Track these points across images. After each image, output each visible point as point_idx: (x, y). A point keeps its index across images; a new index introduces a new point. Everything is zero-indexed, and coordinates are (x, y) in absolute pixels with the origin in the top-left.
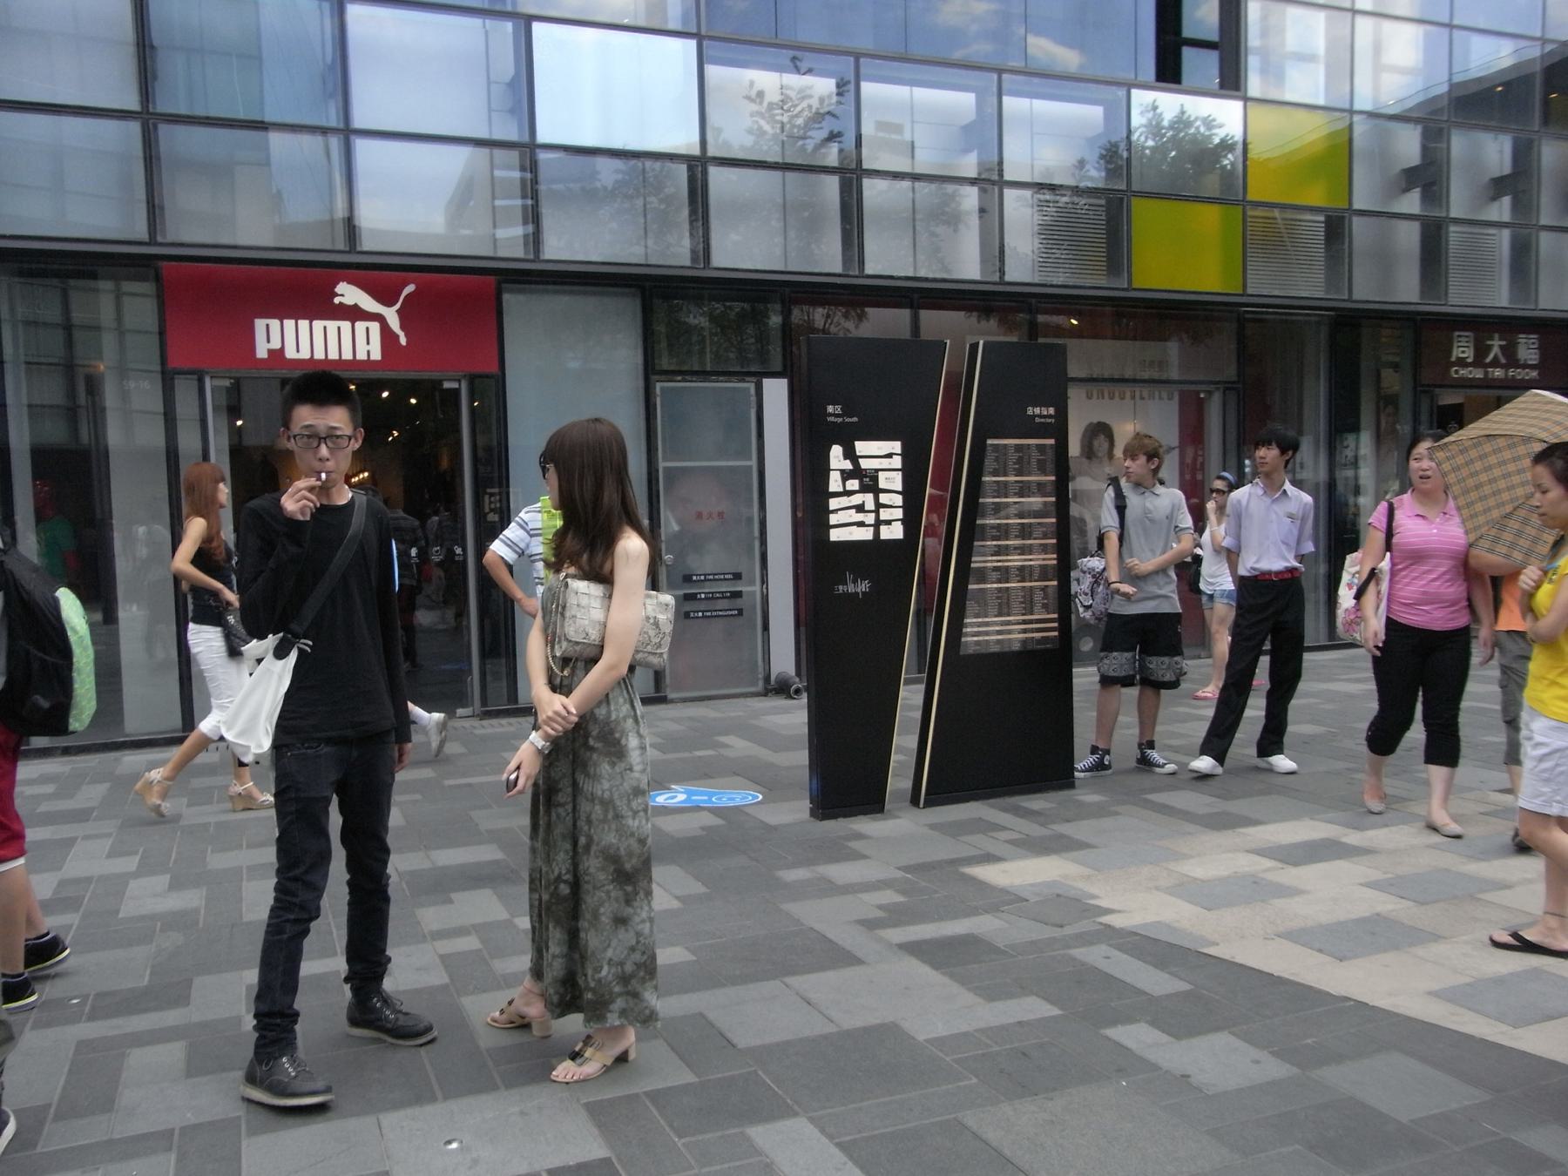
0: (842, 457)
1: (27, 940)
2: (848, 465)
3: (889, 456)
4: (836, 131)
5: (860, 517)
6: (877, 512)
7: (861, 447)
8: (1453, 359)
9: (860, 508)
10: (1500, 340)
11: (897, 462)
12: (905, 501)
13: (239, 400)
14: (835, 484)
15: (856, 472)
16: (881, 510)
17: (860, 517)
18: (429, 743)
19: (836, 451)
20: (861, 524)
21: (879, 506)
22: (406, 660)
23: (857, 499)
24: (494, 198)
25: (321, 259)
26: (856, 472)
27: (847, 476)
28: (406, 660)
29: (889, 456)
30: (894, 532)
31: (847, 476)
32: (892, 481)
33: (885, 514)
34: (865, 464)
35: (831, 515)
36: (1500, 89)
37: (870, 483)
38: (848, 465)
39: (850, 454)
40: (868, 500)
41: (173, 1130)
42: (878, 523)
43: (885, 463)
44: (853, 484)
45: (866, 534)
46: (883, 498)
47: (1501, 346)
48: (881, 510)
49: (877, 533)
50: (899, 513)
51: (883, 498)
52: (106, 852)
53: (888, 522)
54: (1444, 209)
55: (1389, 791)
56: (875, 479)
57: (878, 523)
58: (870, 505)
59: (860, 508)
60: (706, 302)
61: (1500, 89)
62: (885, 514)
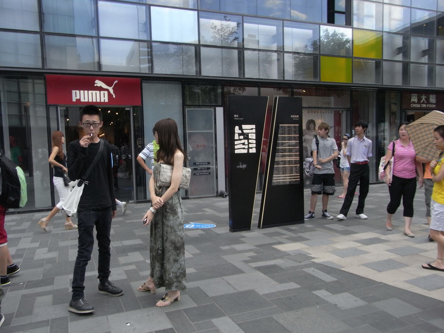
0: (238, 130)
1: (8, 266)
2: (240, 132)
3: (252, 129)
4: (237, 37)
5: (243, 146)
6: (248, 145)
7: (244, 127)
8: (412, 102)
9: (244, 144)
10: (425, 96)
11: (254, 131)
12: (256, 142)
13: (68, 113)
14: (236, 137)
15: (242, 134)
16: (250, 144)
17: (243, 146)
19: (237, 128)
20: (244, 148)
21: (249, 143)
22: (115, 187)
23: (243, 141)
25: (91, 73)
26: (242, 134)
27: (240, 135)
28: (115, 187)
29: (252, 129)
30: (253, 151)
31: (240, 135)
32: (253, 136)
33: (250, 146)
34: (245, 131)
35: (235, 146)
36: (425, 25)
37: (246, 137)
38: (240, 132)
39: (241, 129)
40: (246, 142)
41: (49, 320)
42: (249, 148)
43: (251, 131)
44: (242, 137)
45: (245, 151)
46: (250, 141)
47: (425, 98)
48: (250, 144)
49: (248, 151)
50: (255, 145)
51: (250, 141)
52: (30, 241)
53: (252, 148)
54: (409, 59)
56: (248, 136)
57: (249, 148)
58: (246, 143)
59: (244, 144)
60: (200, 86)
61: (425, 25)
62: (250, 146)
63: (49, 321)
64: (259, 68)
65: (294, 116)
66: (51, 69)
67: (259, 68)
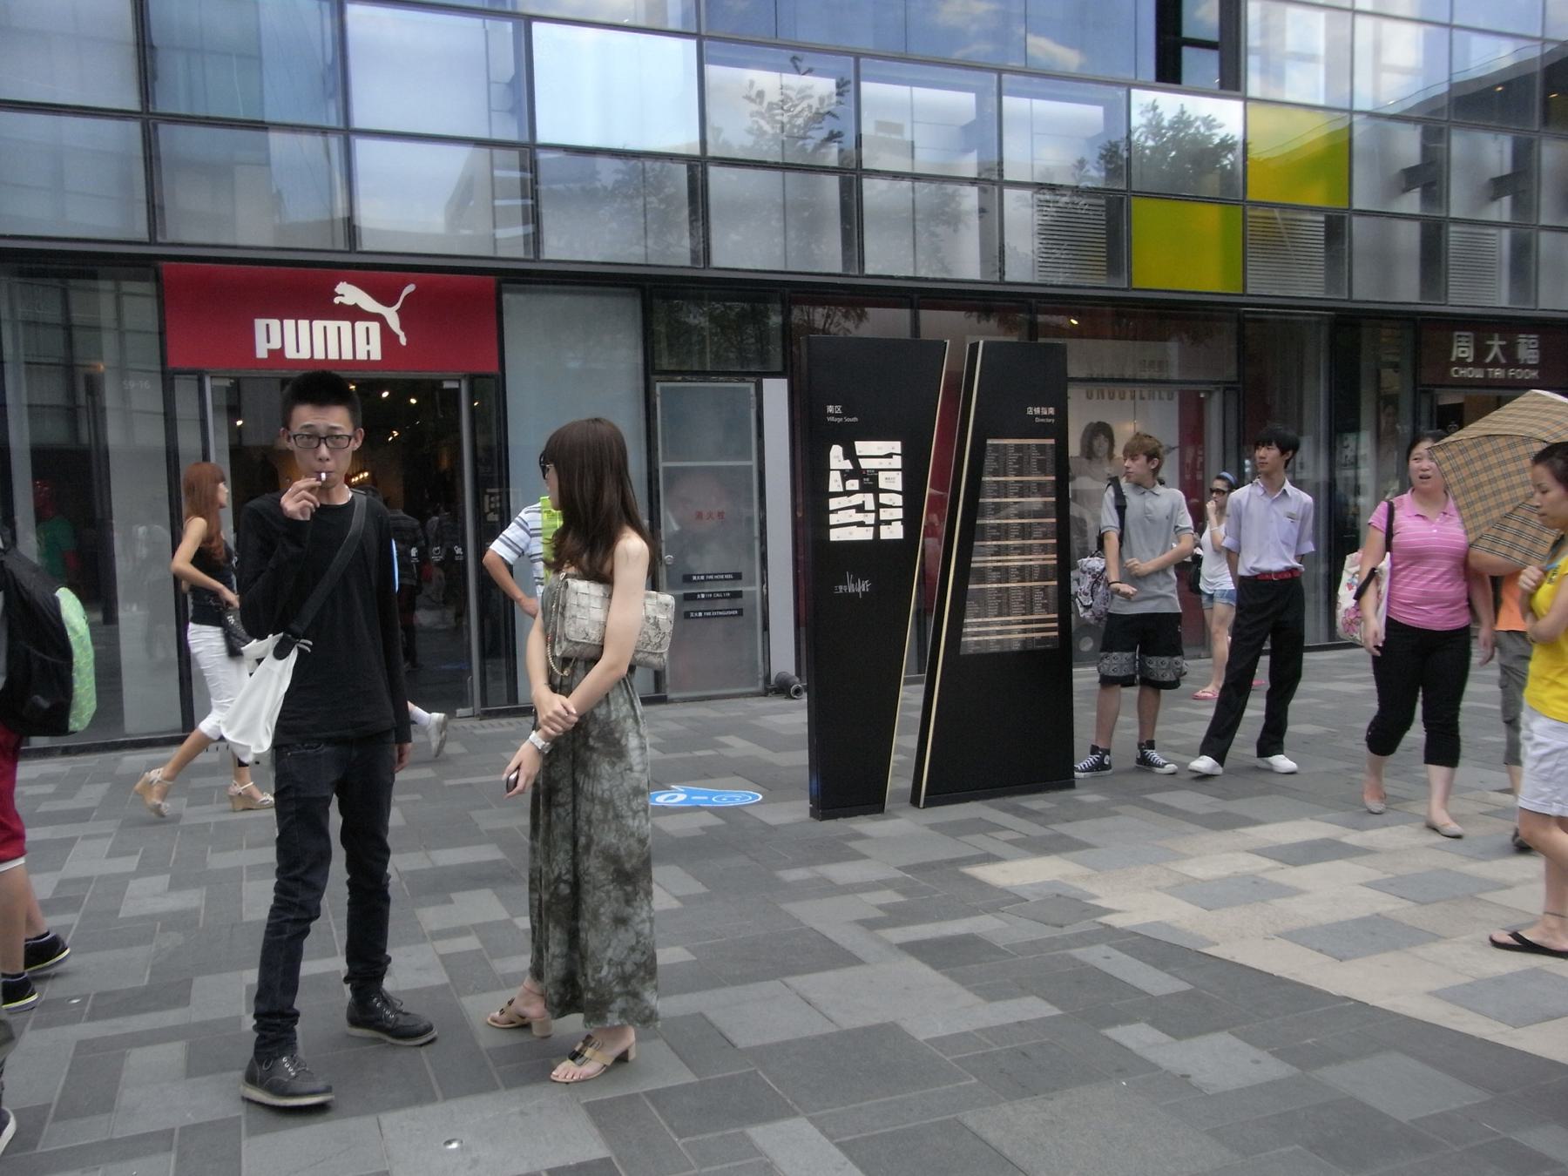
0: (842, 457)
1: (27, 940)
2: (848, 465)
3: (889, 456)
5: (860, 517)
6: (877, 512)
7: (861, 447)
8: (1453, 359)
9: (860, 508)
10: (1500, 340)
11: (897, 462)
12: (905, 501)
13: (239, 400)
14: (835, 484)
15: (856, 472)
16: (881, 510)
17: (860, 517)
18: (429, 743)
19: (836, 451)
20: (861, 524)
21: (879, 506)
22: (406, 660)
23: (857, 499)
24: (494, 198)
25: (321, 259)
26: (856, 472)
27: (847, 476)
28: (406, 660)
29: (889, 456)
30: (894, 532)
31: (847, 476)
32: (892, 481)
33: (885, 514)
34: (865, 464)
35: (831, 515)
37: (870, 483)
38: (848, 465)
39: (850, 454)
40: (868, 500)
42: (878, 523)
43: (885, 463)
44: (853, 484)
45: (866, 534)
46: (883, 498)
47: (1501, 346)
48: (881, 510)
49: (877, 533)
50: (899, 513)
51: (883, 498)
53: (888, 522)
55: (1389, 791)
56: (875, 479)
57: (878, 523)
58: (870, 505)
59: (860, 508)
60: (706, 302)
62: (885, 514)
63: (172, 1135)
64: (914, 239)
65: (1037, 410)
66: (182, 245)
67: (914, 239)
